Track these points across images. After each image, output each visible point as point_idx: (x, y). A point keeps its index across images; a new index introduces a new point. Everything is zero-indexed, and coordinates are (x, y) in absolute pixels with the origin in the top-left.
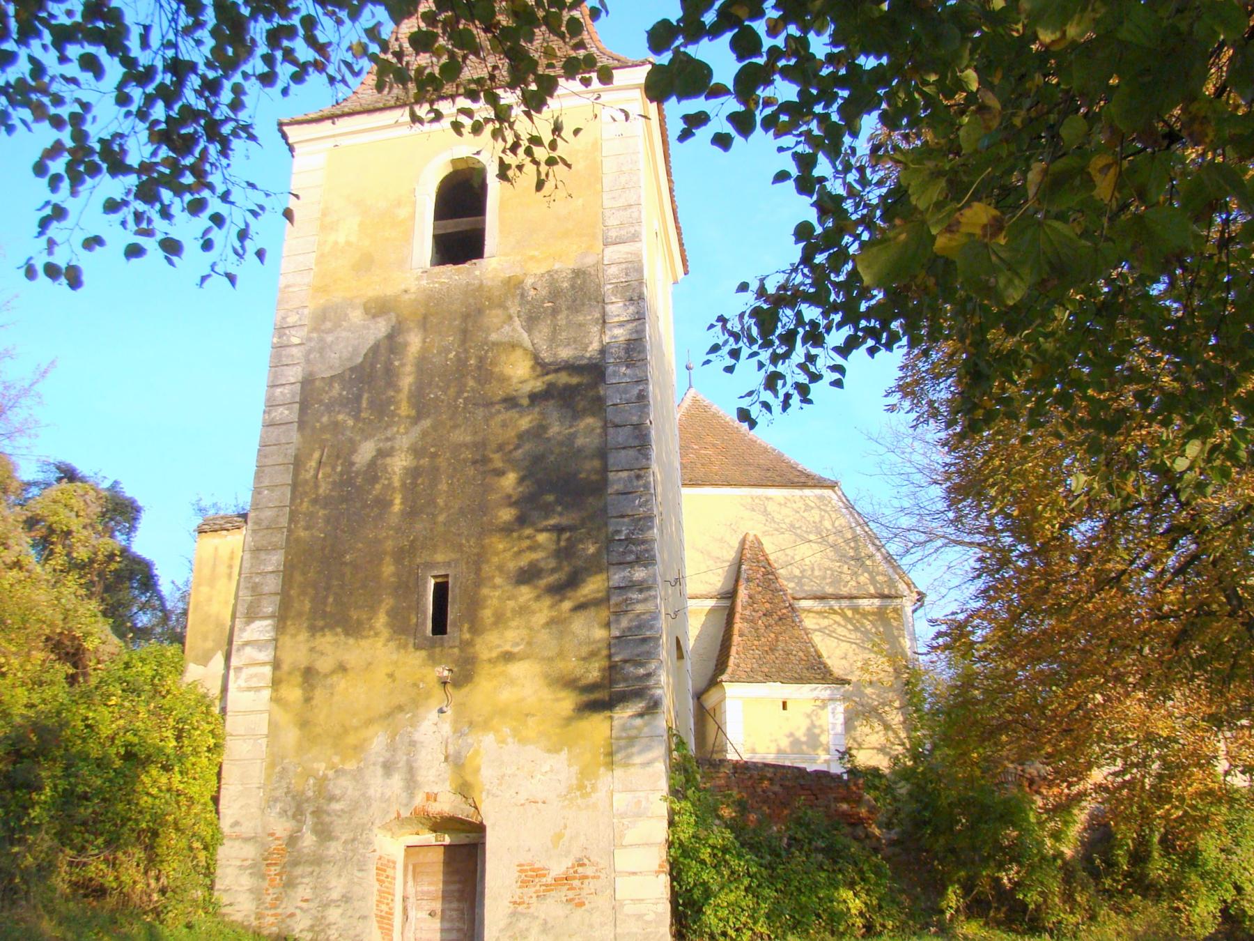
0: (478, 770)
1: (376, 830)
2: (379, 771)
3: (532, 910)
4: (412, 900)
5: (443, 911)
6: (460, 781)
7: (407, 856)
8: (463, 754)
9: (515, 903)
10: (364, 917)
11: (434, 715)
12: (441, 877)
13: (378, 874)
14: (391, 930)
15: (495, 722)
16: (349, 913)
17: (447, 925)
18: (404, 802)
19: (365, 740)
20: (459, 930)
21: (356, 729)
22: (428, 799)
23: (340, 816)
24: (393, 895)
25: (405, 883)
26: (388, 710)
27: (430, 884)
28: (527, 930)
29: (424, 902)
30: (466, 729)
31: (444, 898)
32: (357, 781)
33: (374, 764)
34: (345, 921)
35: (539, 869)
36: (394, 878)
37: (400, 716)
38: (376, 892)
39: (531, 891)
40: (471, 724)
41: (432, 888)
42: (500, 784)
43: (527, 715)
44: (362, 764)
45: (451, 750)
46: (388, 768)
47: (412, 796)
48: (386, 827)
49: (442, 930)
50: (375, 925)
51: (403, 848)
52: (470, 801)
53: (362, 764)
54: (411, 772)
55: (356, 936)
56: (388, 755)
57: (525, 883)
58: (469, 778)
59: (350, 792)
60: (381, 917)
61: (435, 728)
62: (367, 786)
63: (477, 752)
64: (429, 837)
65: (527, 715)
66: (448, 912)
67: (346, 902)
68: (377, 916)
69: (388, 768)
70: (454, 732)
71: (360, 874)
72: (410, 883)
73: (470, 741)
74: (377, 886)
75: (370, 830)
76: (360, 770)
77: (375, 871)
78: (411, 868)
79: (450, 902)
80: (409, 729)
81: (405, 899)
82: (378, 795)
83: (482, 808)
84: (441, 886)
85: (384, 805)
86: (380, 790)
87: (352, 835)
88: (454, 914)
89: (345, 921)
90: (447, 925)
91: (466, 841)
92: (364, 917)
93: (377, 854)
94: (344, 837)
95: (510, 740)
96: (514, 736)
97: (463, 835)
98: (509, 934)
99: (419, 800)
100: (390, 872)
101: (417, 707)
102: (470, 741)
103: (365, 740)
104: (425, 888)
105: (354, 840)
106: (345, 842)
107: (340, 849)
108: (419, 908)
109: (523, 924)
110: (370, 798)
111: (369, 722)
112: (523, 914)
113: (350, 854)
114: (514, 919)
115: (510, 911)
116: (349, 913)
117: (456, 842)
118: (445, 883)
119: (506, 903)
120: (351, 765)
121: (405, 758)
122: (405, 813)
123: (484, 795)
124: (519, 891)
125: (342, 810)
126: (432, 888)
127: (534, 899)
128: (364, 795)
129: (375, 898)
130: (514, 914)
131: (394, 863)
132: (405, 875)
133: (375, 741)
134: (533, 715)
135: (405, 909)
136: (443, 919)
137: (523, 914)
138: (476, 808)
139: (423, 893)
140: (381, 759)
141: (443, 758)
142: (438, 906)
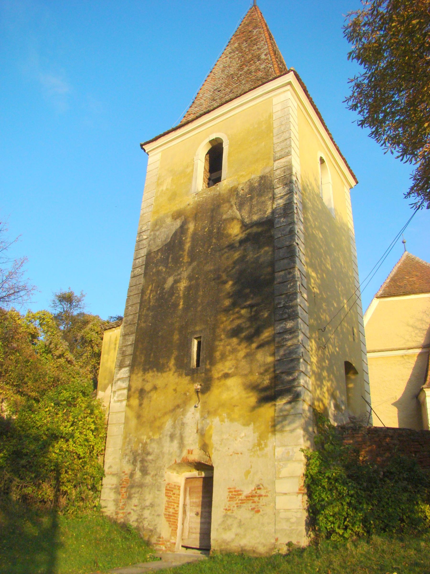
0: (211, 437)
1: (166, 470)
2: (168, 439)
3: (234, 514)
5: (202, 512)
7: (186, 483)
9: (226, 510)
10: (159, 515)
12: (201, 494)
16: (153, 513)
21: (160, 418)
22: (189, 453)
26: (173, 408)
28: (231, 525)
30: (206, 415)
31: (202, 506)
35: (238, 491)
36: (179, 495)
39: (234, 503)
40: (209, 413)
45: (199, 426)
46: (172, 437)
47: (181, 452)
48: (170, 468)
49: (201, 523)
53: (161, 436)
54: (182, 438)
55: (155, 525)
57: (231, 498)
58: (207, 442)
59: (156, 450)
62: (163, 447)
63: (211, 427)
64: (195, 473)
65: (234, 406)
68: (165, 514)
69: (172, 437)
70: (201, 417)
71: (158, 493)
72: (188, 497)
75: (163, 469)
76: (160, 439)
78: (188, 489)
80: (182, 417)
81: (184, 505)
82: (167, 451)
83: (213, 457)
84: (201, 499)
87: (155, 472)
92: (159, 515)
94: (152, 473)
95: (226, 420)
96: (228, 418)
99: (185, 453)
103: (163, 423)
104: (194, 500)
105: (156, 475)
106: (153, 476)
108: (191, 510)
109: (229, 521)
111: (165, 414)
113: (154, 482)
115: (224, 514)
116: (153, 513)
120: (156, 437)
121: (179, 432)
122: (179, 461)
124: (228, 503)
125: (152, 460)
127: (236, 507)
128: (161, 451)
130: (225, 516)
133: (167, 423)
134: (237, 406)
136: (201, 517)
137: (230, 516)
138: (210, 457)
140: (169, 433)
142: (199, 510)
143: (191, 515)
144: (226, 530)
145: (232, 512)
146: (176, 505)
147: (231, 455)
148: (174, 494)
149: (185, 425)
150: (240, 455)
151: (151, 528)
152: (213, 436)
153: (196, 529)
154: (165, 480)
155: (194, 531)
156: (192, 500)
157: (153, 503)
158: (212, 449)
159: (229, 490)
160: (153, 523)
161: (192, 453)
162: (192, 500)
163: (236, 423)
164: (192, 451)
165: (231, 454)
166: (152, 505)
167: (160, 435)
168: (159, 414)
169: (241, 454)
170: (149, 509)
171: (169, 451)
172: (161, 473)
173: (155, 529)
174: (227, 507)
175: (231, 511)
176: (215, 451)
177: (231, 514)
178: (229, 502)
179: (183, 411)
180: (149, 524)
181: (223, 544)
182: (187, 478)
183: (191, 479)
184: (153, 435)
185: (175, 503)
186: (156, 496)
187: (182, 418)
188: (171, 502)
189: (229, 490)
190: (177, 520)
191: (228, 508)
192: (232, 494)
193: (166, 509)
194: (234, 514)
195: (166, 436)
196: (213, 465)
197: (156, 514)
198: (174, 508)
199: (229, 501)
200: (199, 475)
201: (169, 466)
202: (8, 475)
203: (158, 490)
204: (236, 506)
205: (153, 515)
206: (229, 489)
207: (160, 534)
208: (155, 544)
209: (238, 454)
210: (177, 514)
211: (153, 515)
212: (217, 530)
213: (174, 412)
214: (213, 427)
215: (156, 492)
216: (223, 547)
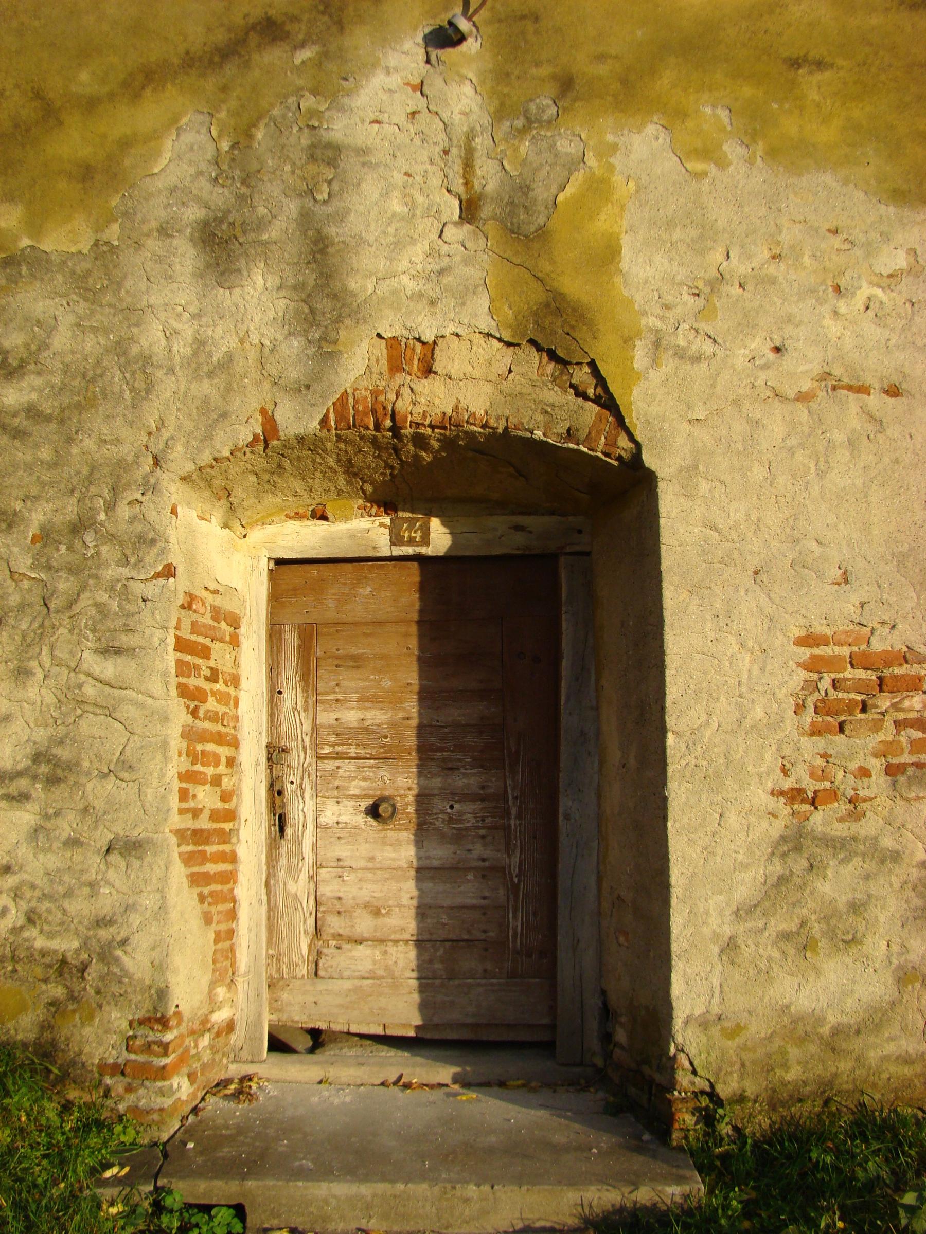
1: (174, 491)
3: (869, 826)
4: (297, 758)
5: (423, 799)
6: (537, 295)
7: (276, 598)
8: (541, 193)
9: (795, 795)
11: (332, 133)
12: (411, 676)
13: (183, 668)
14: (229, 878)
15: (666, 79)
16: (66, 827)
17: (441, 853)
18: (294, 374)
19: (125, 144)
20: (488, 872)
21: (91, 105)
22: (396, 366)
23: (19, 434)
24: (235, 744)
25: (275, 693)
26: (220, 37)
27: (365, 700)
28: (855, 908)
29: (347, 767)
30: (545, 104)
32: (91, 295)
33: (164, 232)
34: (52, 861)
35: (890, 659)
36: (235, 681)
37: (273, 56)
38: (176, 743)
41: (376, 716)
42: (706, 312)
43: (795, 63)
44: (113, 232)
49: (423, 872)
50: (179, 872)
51: (264, 565)
52: (582, 376)
53: (113, 232)
55: (102, 922)
56: (221, 197)
59: (61, 340)
60: (199, 836)
61: (416, 101)
65: (795, 63)
66: (440, 804)
67: (53, 781)
68: (180, 834)
70: (499, 115)
71: (108, 668)
72: (292, 697)
73: (567, 146)
74: (180, 717)
75: (151, 488)
77: (171, 657)
78: (291, 639)
79: (449, 769)
80: (309, 102)
82: (181, 348)
84: (412, 707)
85: (206, 388)
86: (188, 330)
87: (71, 509)
88: (468, 811)
89: (52, 861)
90: (441, 853)
91: (514, 543)
93: (179, 585)
94: (37, 517)
95: (733, 150)
96: (750, 137)
97: (499, 523)
98: (780, 923)
100: (221, 655)
101: (340, 26)
102: (567, 146)
103: (125, 144)
104: (351, 716)
105: (77, 528)
106: (45, 537)
107: (23, 563)
110: (146, 360)
112: (837, 845)
113: (65, 585)
114: (799, 864)
115: (777, 828)
116: (66, 827)
117: (475, 547)
118: (426, 696)
119: (761, 797)
121: (292, 207)
123: (640, 356)
124: (810, 747)
125: (32, 412)
126: (376, 716)
127: (878, 782)
128: (120, 348)
129: (176, 765)
131: (235, 622)
132: (273, 669)
133: (168, 147)
134: (820, 65)
135: (276, 792)
139: (342, 733)
140: (193, 213)
141: (453, 209)
143: (329, 815)
144: (807, 946)
145: (855, 815)
146: (224, 752)
147: (803, 397)
148: (214, 676)
149: (349, 163)
150: (875, 401)
151: (67, 945)
152: (626, 253)
153: (377, 913)
154: (169, 572)
155: (364, 924)
156: (326, 717)
157: (64, 753)
158: (628, 341)
159: (805, 653)
160: (79, 907)
161: (428, 371)
162: (326, 717)
163: (828, 179)
164: (430, 348)
165: (806, 385)
166: (55, 762)
167: (99, 229)
168: (84, 76)
169: (893, 391)
170: (23, 797)
171: (200, 344)
172: (124, 511)
173: (106, 954)
174: (802, 778)
175: (842, 807)
176: (655, 362)
177: (839, 830)
178: (820, 743)
179: (318, 63)
180: (31, 918)
181: (794, 1052)
182: (280, 562)
183: (314, 570)
184: (35, 226)
185: (220, 739)
186: (90, 690)
187: (314, 113)
188: (204, 737)
189: (805, 653)
190: (232, 858)
191: (810, 786)
192: (835, 684)
193: (184, 795)
194: (869, 826)
195: (164, 232)
196: (649, 459)
197: (103, 837)
198: (216, 781)
199: (815, 732)
200: (396, 540)
201: (206, 458)
202: (720, 798)
203: (110, 651)
204: (876, 765)
205: (73, 843)
206: (808, 640)
207: (162, 994)
208: (119, 1070)
209: (863, 389)
210: (231, 816)
211: (73, 843)
212: (730, 947)
213: (230, 69)
214: (623, 188)
215: (91, 661)
216: (793, 1074)
